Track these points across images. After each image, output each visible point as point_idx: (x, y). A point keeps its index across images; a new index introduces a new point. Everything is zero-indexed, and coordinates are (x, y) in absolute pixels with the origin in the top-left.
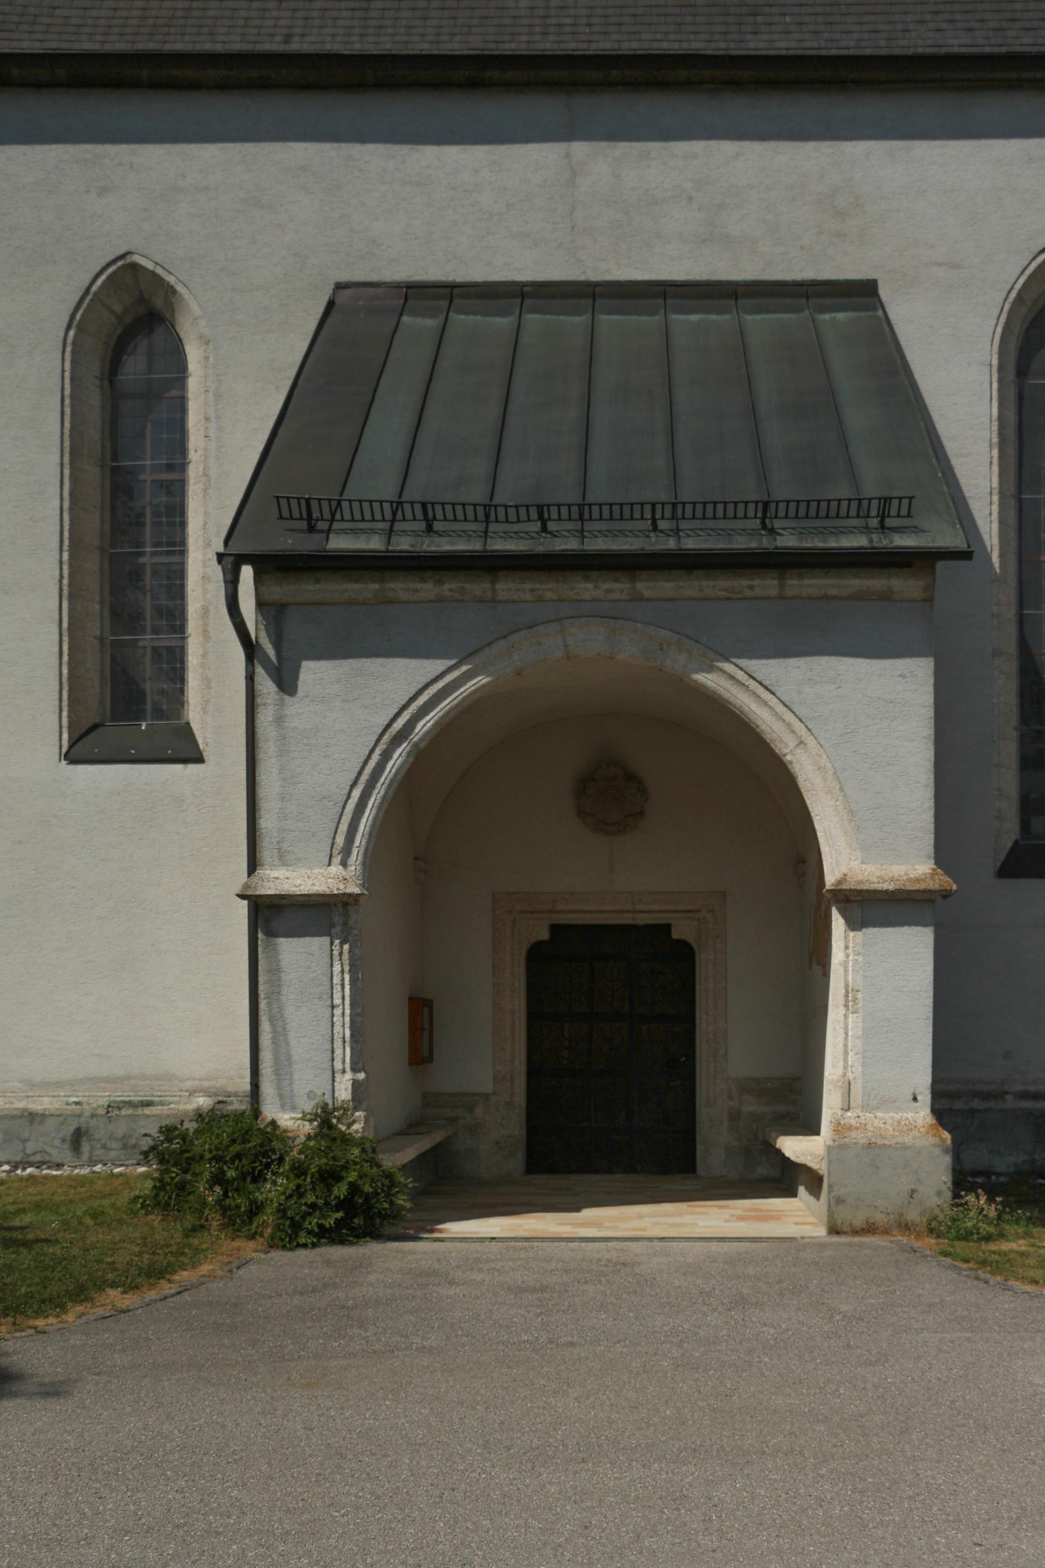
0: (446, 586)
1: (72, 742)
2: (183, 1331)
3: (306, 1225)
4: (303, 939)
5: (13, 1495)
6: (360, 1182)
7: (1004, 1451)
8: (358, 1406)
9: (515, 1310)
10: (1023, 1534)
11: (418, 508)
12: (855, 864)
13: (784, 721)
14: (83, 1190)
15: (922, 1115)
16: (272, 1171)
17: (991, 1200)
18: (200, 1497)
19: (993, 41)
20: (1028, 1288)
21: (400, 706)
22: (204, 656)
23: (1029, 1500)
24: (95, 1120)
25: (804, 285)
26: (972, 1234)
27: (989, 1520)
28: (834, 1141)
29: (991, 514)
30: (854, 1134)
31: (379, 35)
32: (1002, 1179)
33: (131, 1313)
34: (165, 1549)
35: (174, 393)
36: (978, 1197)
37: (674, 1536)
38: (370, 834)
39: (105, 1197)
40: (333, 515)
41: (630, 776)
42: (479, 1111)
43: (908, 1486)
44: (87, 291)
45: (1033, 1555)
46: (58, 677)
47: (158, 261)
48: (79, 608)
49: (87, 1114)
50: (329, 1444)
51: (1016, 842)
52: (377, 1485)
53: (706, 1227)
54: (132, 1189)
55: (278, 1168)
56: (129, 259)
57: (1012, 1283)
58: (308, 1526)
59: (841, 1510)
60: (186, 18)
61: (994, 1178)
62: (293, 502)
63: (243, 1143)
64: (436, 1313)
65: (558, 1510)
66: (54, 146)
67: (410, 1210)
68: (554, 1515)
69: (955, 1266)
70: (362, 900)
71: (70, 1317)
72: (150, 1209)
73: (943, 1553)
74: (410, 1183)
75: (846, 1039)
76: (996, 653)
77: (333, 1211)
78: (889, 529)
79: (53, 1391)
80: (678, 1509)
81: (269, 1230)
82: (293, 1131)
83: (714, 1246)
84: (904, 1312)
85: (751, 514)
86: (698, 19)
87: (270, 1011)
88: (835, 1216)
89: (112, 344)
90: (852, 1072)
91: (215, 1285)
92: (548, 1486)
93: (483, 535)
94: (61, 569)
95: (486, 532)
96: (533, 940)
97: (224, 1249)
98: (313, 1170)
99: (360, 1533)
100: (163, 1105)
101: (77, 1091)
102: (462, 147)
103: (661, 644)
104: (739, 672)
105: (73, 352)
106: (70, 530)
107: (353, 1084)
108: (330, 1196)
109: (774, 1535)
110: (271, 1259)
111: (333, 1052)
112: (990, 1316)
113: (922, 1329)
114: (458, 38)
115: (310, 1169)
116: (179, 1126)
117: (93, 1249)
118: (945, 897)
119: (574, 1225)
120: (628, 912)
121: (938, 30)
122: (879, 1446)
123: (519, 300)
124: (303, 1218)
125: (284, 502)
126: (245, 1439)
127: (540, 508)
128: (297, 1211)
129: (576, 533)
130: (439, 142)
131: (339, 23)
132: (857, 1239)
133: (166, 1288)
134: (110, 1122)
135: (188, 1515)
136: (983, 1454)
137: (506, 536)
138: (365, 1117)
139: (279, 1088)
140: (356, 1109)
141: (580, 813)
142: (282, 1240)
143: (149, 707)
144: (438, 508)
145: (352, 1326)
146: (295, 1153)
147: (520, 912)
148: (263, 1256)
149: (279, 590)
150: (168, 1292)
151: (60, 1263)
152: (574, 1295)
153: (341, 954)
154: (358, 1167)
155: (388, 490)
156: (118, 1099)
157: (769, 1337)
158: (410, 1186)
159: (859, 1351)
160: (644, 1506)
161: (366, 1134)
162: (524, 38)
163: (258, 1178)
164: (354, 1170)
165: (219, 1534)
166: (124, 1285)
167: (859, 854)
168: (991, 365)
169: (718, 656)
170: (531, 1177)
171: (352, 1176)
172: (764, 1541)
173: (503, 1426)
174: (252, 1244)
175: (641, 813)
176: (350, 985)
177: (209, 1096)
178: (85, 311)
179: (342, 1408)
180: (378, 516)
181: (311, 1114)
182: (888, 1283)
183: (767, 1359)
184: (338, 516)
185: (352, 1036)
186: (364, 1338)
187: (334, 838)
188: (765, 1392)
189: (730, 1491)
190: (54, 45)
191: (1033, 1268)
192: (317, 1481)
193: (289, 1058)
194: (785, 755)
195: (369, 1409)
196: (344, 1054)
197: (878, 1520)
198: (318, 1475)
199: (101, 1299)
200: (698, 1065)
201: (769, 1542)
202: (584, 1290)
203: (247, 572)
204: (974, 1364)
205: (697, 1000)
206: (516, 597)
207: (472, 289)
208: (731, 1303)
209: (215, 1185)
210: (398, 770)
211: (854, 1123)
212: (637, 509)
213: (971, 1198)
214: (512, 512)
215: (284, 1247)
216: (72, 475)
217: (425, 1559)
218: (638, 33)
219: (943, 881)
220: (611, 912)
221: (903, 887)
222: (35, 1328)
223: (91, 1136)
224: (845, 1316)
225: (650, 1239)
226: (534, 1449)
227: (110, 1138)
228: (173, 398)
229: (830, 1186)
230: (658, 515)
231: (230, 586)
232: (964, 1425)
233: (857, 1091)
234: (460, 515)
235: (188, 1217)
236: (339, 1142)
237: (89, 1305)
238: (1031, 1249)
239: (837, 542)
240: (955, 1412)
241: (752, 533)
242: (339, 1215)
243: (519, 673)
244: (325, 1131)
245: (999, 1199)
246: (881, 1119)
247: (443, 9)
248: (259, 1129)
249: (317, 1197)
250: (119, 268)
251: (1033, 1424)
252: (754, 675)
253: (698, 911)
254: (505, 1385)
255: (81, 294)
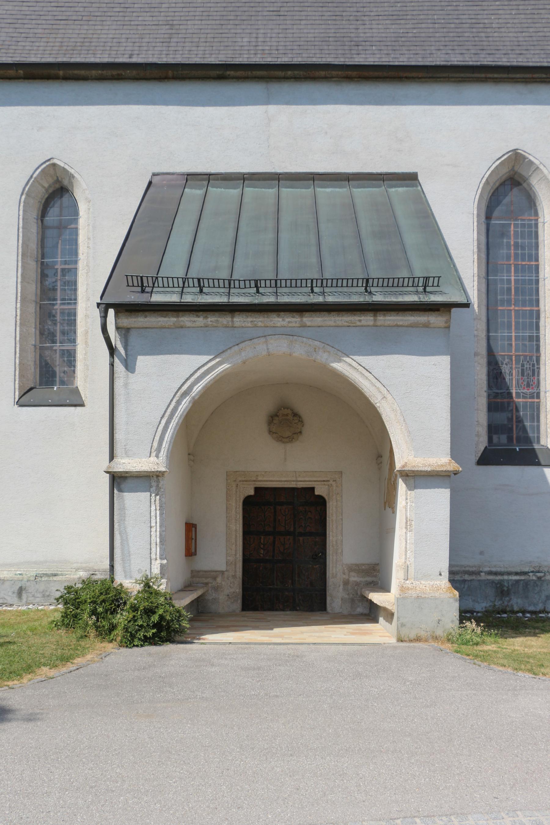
0: (209, 319)
1: (20, 396)
2: (82, 688)
3: (138, 635)
4: (136, 493)
5: (7, 770)
6: (165, 615)
7: (501, 750)
8: (174, 727)
9: (246, 679)
10: (517, 793)
11: (196, 281)
12: (411, 458)
13: (376, 386)
14: (24, 617)
15: (444, 582)
16: (121, 609)
17: (478, 625)
18: (101, 773)
19: (474, 59)
20: (501, 668)
21: (186, 378)
22: (85, 354)
23: (517, 775)
24: (29, 583)
25: (382, 175)
26: (469, 641)
27: (500, 785)
28: (400, 595)
29: (473, 286)
30: (410, 592)
31: (175, 54)
32: (479, 614)
33: (55, 679)
34: (87, 799)
35: (73, 226)
36: (471, 622)
37: (343, 794)
38: (170, 442)
39: (35, 621)
40: (154, 284)
41: (295, 415)
42: (219, 580)
43: (457, 768)
44: (31, 177)
45: (524, 803)
46: (14, 364)
47: (66, 163)
48: (25, 330)
49: (25, 580)
50: (162, 746)
51: (486, 447)
52: (189, 767)
53: (335, 638)
54: (48, 617)
55: (124, 607)
56: (51, 162)
57: (492, 666)
58: (157, 788)
59: (425, 781)
60: (82, 46)
61: (475, 614)
62: (135, 278)
63: (106, 594)
64: (207, 680)
65: (282, 780)
66: (16, 107)
67: (188, 629)
68: (281, 783)
69: (463, 658)
70: (166, 474)
71: (25, 681)
72: (59, 627)
73: (479, 802)
74: (189, 615)
75: (406, 544)
76: (476, 354)
77: (151, 629)
78: (428, 292)
79: (31, 718)
80: (343, 780)
81: (120, 638)
82: (131, 589)
83: (341, 647)
84: (441, 681)
85: (360, 284)
86: (330, 47)
87: (120, 529)
88: (401, 633)
89: (43, 202)
90: (409, 561)
91: (95, 665)
92: (275, 768)
93: (228, 294)
94: (16, 311)
95: (229, 293)
96: (246, 495)
97: (97, 647)
98: (141, 608)
99: (184, 791)
100: (63, 575)
101: (20, 568)
102: (215, 107)
103: (315, 348)
104: (354, 362)
105: (24, 206)
106: (21, 292)
107: (160, 566)
108: (150, 621)
109: (393, 793)
110: (121, 652)
111: (151, 549)
112: (484, 683)
113: (451, 689)
114: (213, 56)
115: (140, 608)
116: (74, 586)
117: (33, 647)
118: (455, 474)
119: (270, 637)
120: (294, 481)
121: (447, 54)
122: (438, 748)
123: (242, 181)
124: (136, 632)
125: (130, 278)
126: (120, 743)
127: (256, 281)
128: (133, 629)
129: (273, 294)
130: (203, 105)
131: (156, 49)
132: (412, 644)
133: (70, 666)
134: (36, 583)
135: (96, 781)
136: (491, 752)
137: (239, 295)
138: (167, 582)
139: (124, 567)
140: (162, 578)
141: (270, 432)
142: (126, 643)
143: (58, 379)
144: (206, 281)
145: (166, 687)
146: (132, 600)
147: (240, 481)
148: (117, 651)
149: (127, 321)
150: (72, 669)
151: (17, 654)
152: (274, 672)
153: (155, 501)
154: (163, 607)
155: (180, 272)
156: (41, 572)
157: (375, 693)
158: (189, 616)
159: (421, 700)
160: (325, 779)
161: (167, 591)
162: (245, 56)
163: (114, 612)
164: (161, 608)
165: (113, 791)
166: (50, 665)
167: (413, 452)
168: (473, 214)
169: (343, 355)
170: (244, 613)
171: (161, 612)
172: (389, 796)
173: (248, 738)
174: (111, 645)
175: (300, 432)
176: (160, 516)
177: (86, 571)
178: (30, 187)
179: (166, 728)
180: (176, 285)
181: (140, 581)
182: (431, 666)
183: (376, 704)
184: (156, 285)
185: (160, 541)
186: (172, 693)
187: (152, 443)
188: (378, 721)
189: (368, 771)
190: (18, 59)
191: (502, 659)
192: (158, 765)
193: (129, 552)
194: (376, 404)
195: (180, 728)
196: (156, 551)
197: (444, 786)
198: (159, 761)
199: (39, 671)
200: (328, 557)
201: (391, 797)
202: (279, 669)
203: (111, 312)
204: (479, 706)
205: (328, 524)
206: (243, 325)
207: (219, 176)
208: (354, 676)
209: (92, 615)
210: (184, 410)
211: (410, 587)
212: (304, 282)
213: (468, 624)
214: (242, 283)
215: (127, 646)
216: (22, 266)
217: (219, 805)
218: (301, 54)
219: (454, 466)
220: (285, 481)
221: (435, 469)
222: (8, 686)
223: (27, 590)
224: (411, 682)
225: (309, 644)
226: (266, 749)
227: (36, 592)
228: (72, 228)
229: (398, 618)
230: (314, 285)
231: (103, 319)
232: (479, 738)
233: (412, 570)
234: (216, 284)
235: (79, 631)
236: (153, 594)
237: (33, 675)
238: (499, 649)
239: (403, 299)
240: (474, 731)
241: (361, 294)
242: (154, 631)
243: (244, 363)
244: (147, 589)
245: (482, 624)
246: (423, 584)
247: (206, 42)
248: (114, 588)
249: (143, 622)
250: (47, 166)
251: (514, 737)
252: (361, 364)
253: (329, 481)
254: (247, 717)
255: (28, 178)
